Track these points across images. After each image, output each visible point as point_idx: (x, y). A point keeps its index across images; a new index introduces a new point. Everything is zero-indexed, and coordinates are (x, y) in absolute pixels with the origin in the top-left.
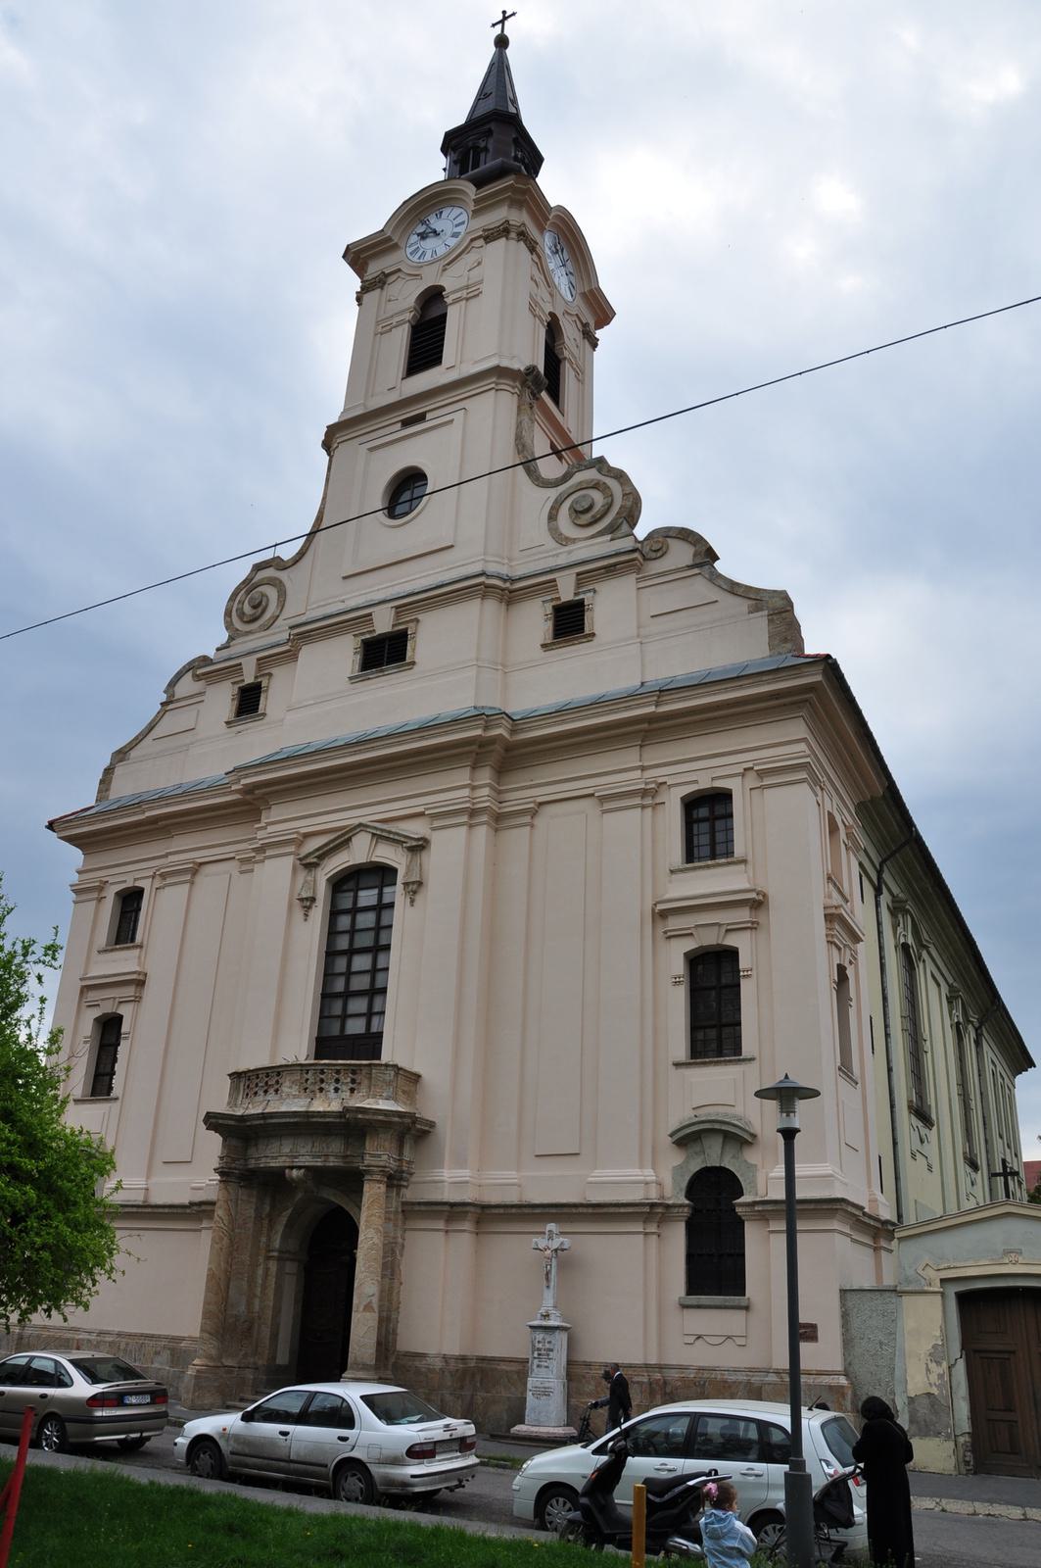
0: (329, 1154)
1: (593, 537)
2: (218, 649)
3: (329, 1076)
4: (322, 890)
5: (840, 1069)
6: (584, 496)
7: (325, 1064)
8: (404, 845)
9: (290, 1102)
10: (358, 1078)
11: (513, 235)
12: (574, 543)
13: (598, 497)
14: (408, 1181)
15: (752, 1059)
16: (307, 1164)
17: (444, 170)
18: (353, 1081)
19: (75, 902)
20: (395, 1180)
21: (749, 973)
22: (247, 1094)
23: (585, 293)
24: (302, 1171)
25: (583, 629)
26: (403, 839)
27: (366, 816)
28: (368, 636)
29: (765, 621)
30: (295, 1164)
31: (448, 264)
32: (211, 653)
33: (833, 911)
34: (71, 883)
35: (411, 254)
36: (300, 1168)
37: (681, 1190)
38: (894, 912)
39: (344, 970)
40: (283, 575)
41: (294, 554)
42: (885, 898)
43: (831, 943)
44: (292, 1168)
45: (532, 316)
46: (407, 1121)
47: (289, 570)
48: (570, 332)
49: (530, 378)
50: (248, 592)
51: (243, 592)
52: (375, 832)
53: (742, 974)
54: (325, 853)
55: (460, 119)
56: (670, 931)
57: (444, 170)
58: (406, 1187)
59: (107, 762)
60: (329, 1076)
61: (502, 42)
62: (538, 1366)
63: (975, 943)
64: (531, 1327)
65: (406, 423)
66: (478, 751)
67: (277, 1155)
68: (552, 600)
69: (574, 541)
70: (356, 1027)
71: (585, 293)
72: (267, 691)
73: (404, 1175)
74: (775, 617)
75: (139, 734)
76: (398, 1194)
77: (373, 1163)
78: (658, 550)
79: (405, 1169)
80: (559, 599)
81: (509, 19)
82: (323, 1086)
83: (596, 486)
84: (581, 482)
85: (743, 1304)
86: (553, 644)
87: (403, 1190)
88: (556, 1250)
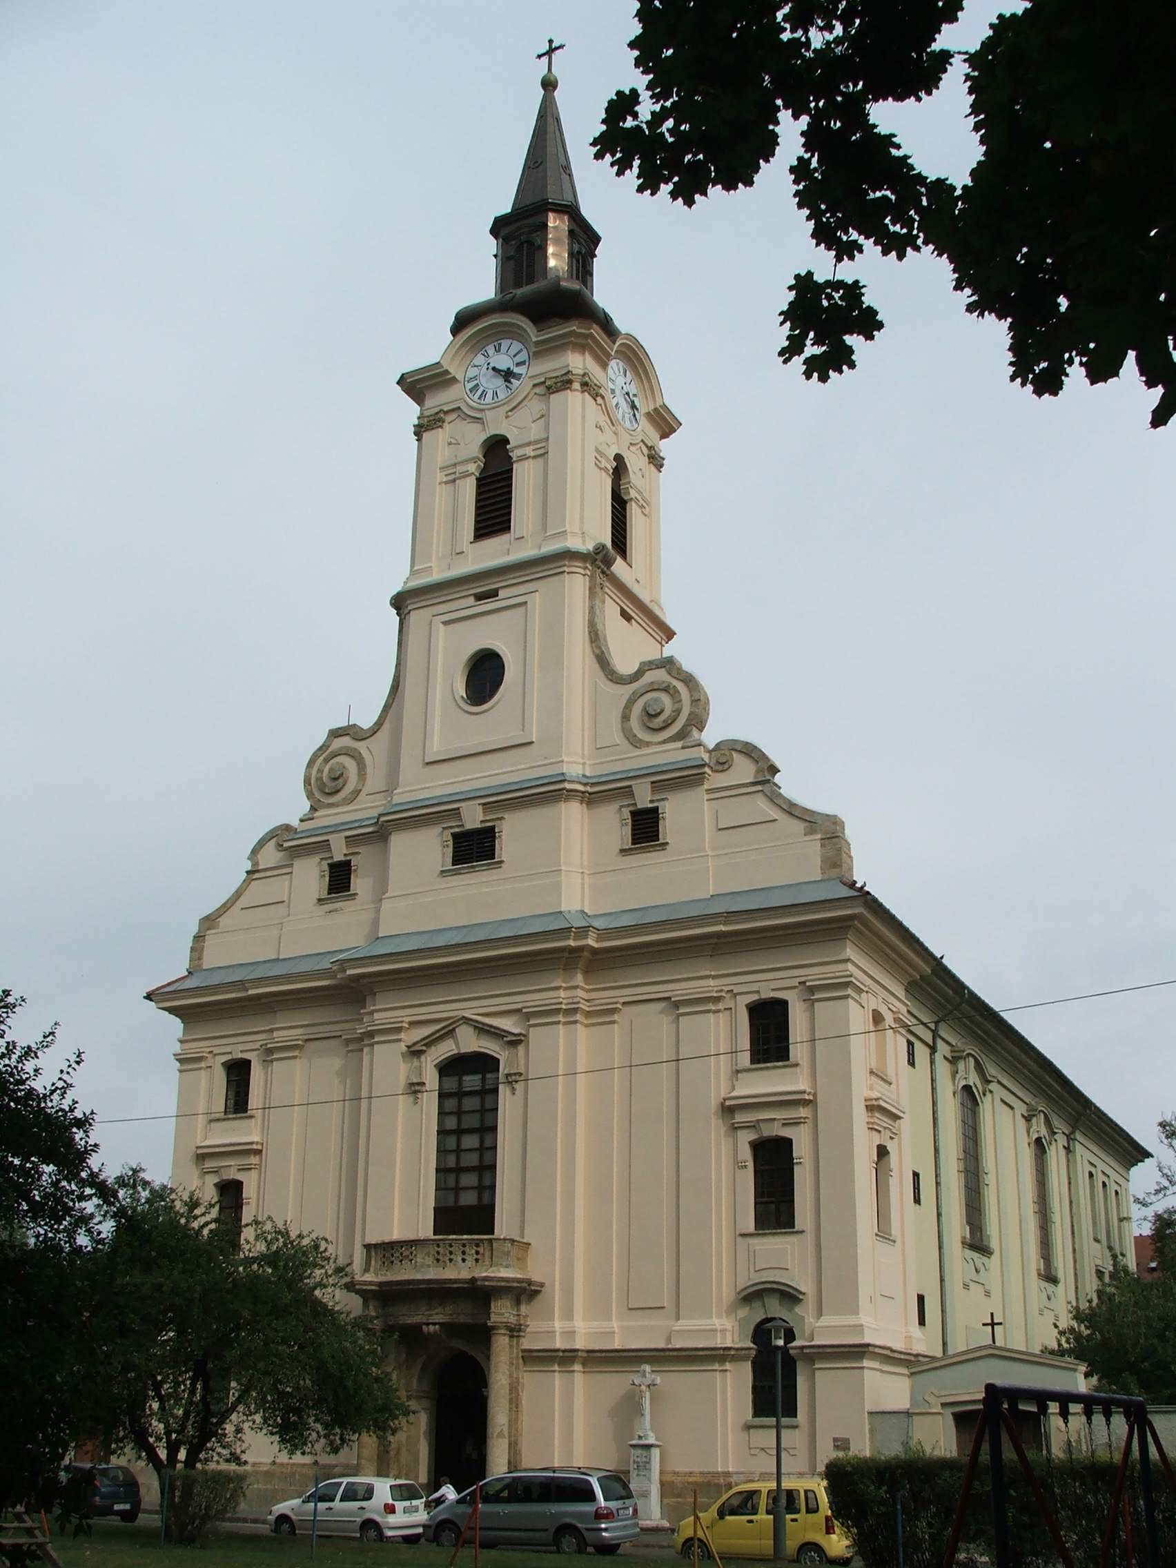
0: (463, 1314)
1: (664, 742)
2: (302, 821)
3: (457, 1249)
4: (431, 1078)
5: (877, 1235)
6: (656, 700)
7: (453, 1240)
8: (505, 1039)
9: (425, 1270)
10: (481, 1250)
11: (576, 385)
12: (648, 746)
13: (666, 699)
14: (524, 1332)
15: (802, 1232)
16: (441, 1321)
17: (495, 256)
18: (477, 1253)
19: (180, 1071)
20: (515, 1331)
21: (801, 1160)
22: (384, 1263)
23: (649, 412)
24: (437, 1327)
25: (658, 835)
26: (503, 1033)
27: (470, 1010)
28: (457, 830)
29: (818, 844)
30: (431, 1321)
31: (511, 411)
32: (295, 823)
33: (874, 1103)
34: (174, 1052)
35: (471, 391)
36: (434, 1324)
37: (748, 1336)
38: (953, 1061)
39: (454, 1147)
40: (361, 746)
41: (371, 724)
42: (942, 1049)
43: (872, 1129)
44: (428, 1324)
45: (598, 470)
46: (525, 1285)
47: (368, 740)
48: (636, 463)
49: (599, 557)
50: (326, 761)
51: (322, 758)
52: (477, 1025)
53: (795, 1161)
54: (431, 1041)
55: (507, 208)
56: (738, 1123)
57: (495, 256)
58: (524, 1337)
59: (195, 929)
60: (457, 1249)
61: (549, 85)
62: (638, 1475)
63: (1052, 1063)
64: (631, 1446)
65: (480, 597)
66: (568, 956)
67: (414, 1316)
68: (629, 805)
69: (648, 744)
70: (469, 1199)
71: (649, 412)
72: (355, 870)
73: (523, 1327)
74: (827, 841)
75: (228, 900)
76: (518, 1343)
77: (499, 1320)
78: (725, 763)
79: (522, 1322)
80: (635, 804)
81: (557, 52)
82: (452, 1257)
83: (666, 689)
84: (652, 683)
85: (795, 1424)
86: (631, 849)
87: (522, 1340)
88: (649, 1386)
